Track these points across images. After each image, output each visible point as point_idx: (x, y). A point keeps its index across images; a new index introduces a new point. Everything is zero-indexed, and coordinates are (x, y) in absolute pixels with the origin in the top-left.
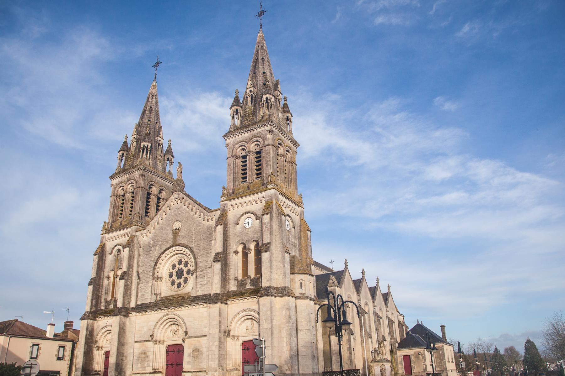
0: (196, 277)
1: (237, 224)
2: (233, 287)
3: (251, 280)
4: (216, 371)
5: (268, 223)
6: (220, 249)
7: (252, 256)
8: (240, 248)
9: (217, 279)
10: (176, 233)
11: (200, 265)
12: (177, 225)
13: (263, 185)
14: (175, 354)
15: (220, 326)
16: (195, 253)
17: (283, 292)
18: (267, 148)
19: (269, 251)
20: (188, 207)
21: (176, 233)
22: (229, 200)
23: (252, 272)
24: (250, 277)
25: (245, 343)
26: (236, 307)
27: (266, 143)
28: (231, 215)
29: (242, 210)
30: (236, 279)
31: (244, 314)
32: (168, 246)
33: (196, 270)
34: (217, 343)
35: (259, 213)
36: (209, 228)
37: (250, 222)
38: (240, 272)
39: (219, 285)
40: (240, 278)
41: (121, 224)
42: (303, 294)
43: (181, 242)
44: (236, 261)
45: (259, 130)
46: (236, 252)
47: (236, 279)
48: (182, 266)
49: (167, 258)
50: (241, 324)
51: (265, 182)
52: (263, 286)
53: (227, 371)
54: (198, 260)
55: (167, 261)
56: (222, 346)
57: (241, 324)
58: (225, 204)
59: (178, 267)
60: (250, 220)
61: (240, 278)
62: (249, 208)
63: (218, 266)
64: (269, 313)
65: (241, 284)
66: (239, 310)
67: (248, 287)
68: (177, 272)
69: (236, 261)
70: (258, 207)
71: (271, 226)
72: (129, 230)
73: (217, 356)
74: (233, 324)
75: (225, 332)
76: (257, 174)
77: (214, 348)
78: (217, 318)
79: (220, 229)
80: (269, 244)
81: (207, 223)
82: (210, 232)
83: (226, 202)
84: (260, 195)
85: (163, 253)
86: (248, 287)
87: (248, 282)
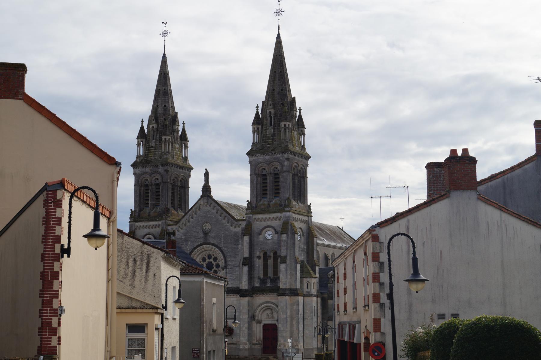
0: (226, 272)
1: (260, 234)
2: (257, 285)
3: (271, 280)
4: (246, 344)
5: (285, 241)
6: (246, 255)
7: (271, 262)
8: (262, 255)
9: (245, 278)
10: (206, 234)
11: (230, 263)
12: (207, 227)
13: (281, 206)
14: (271, 332)
15: (248, 313)
16: (225, 253)
17: (294, 292)
18: (284, 174)
19: (285, 263)
20: (217, 213)
21: (206, 234)
22: (253, 214)
23: (271, 273)
24: (270, 277)
25: (265, 326)
26: (260, 299)
27: (285, 169)
28: (257, 226)
29: (264, 224)
30: (259, 278)
31: (265, 305)
32: (199, 243)
33: (225, 267)
34: (246, 325)
35: (279, 229)
36: (236, 234)
37: (269, 235)
38: (262, 272)
39: (247, 283)
40: (262, 277)
41: (149, 215)
42: (309, 292)
43: (212, 242)
44: (259, 263)
45: (278, 156)
46: (259, 257)
47: (259, 278)
48: (212, 260)
49: (198, 253)
50: (263, 312)
51: (283, 204)
52: (281, 287)
53: (253, 344)
54: (227, 259)
55: (198, 255)
56: (250, 328)
57: (263, 312)
58: (250, 217)
59: (208, 260)
60: (270, 233)
61: (262, 277)
62: (269, 223)
63: (246, 269)
64: (285, 307)
65: (263, 281)
66: (261, 302)
67: (268, 285)
68: (206, 264)
69: (259, 263)
70: (277, 224)
71: (287, 243)
72: (160, 223)
73: (246, 335)
74: (257, 312)
75: (251, 317)
76: (276, 193)
77: (244, 329)
78: (247, 307)
79: (246, 238)
80: (286, 257)
81: (234, 230)
82: (236, 240)
83: (251, 215)
84: (279, 215)
85: (195, 248)
86: (268, 285)
87: (269, 281)
